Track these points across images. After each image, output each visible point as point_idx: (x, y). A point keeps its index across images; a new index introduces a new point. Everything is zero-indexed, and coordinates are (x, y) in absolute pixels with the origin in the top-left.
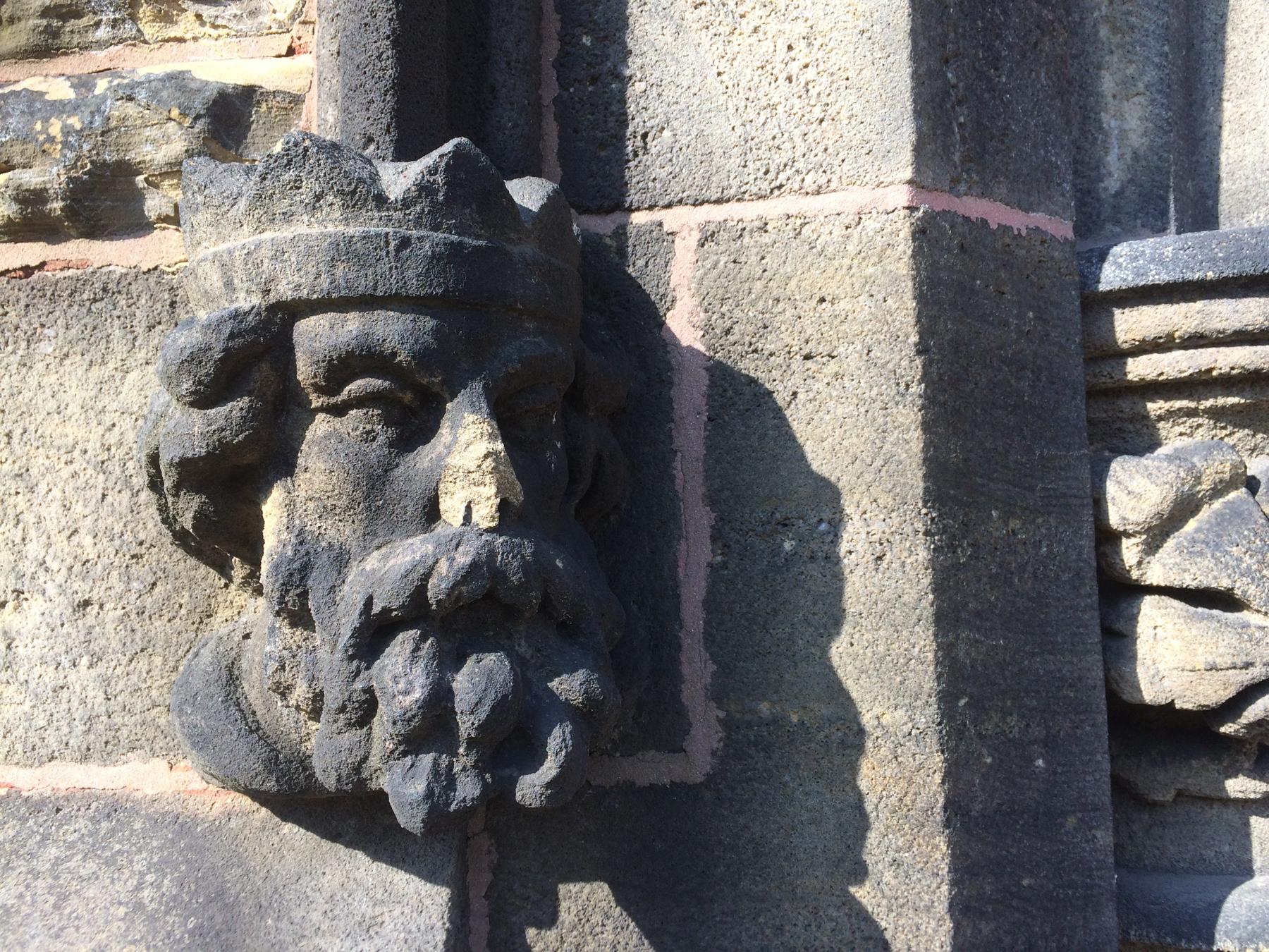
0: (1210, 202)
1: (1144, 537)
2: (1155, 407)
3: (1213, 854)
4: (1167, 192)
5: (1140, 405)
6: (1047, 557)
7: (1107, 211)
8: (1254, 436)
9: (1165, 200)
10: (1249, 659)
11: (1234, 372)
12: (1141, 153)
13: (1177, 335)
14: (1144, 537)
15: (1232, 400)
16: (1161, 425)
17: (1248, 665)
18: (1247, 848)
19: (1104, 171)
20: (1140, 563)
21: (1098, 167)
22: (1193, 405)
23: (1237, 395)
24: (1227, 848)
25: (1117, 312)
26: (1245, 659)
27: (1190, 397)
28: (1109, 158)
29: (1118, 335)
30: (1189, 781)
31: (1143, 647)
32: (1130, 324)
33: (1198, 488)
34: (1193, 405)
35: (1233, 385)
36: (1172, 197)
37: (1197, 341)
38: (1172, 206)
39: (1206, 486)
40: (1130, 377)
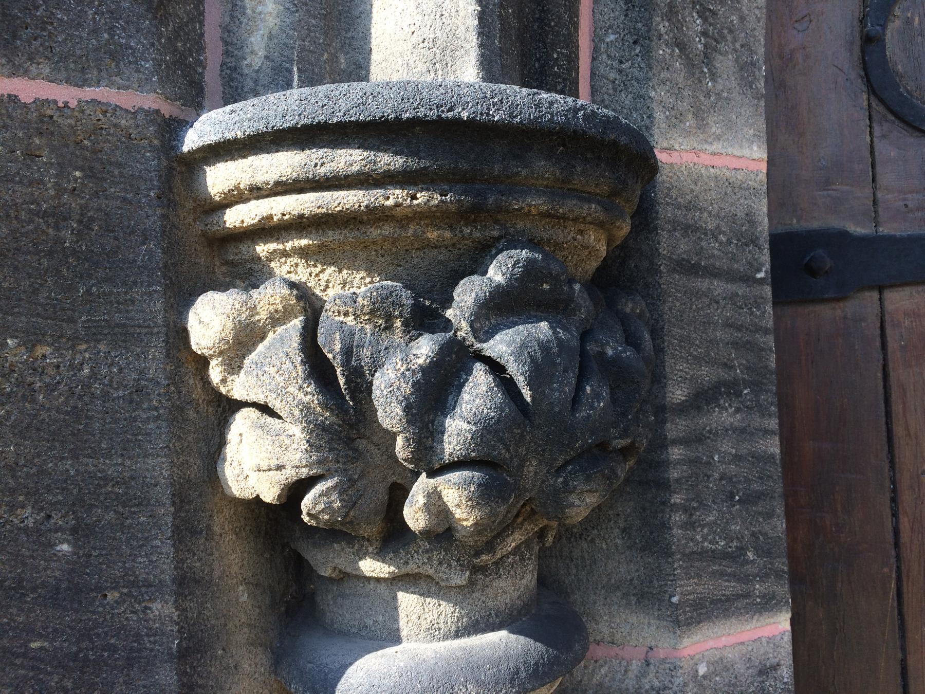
0: (364, 72)
1: (220, 359)
2: (262, 249)
3: (371, 623)
4: (292, 65)
5: (252, 248)
6: (90, 378)
7: (249, 84)
8: (340, 272)
9: (290, 71)
10: (280, 462)
11: (285, 218)
12: (274, 32)
13: (242, 186)
14: (220, 359)
15: (304, 242)
16: (273, 264)
17: (279, 468)
18: (396, 619)
19: (248, 50)
20: (224, 381)
21: (242, 47)
22: (281, 247)
23: (306, 237)
24: (381, 618)
25: (207, 169)
26: (276, 462)
27: (277, 240)
28: (252, 39)
29: (210, 189)
30: (336, 561)
31: (230, 450)
32: (219, 178)
33: (257, 317)
34: (281, 247)
35: (304, 228)
36: (295, 69)
37: (257, 192)
38: (296, 77)
39: (263, 315)
40: (227, 225)
